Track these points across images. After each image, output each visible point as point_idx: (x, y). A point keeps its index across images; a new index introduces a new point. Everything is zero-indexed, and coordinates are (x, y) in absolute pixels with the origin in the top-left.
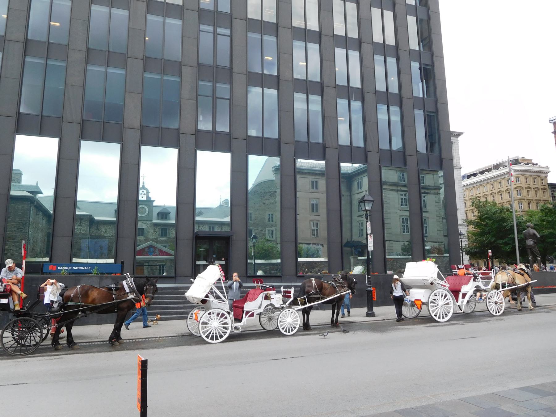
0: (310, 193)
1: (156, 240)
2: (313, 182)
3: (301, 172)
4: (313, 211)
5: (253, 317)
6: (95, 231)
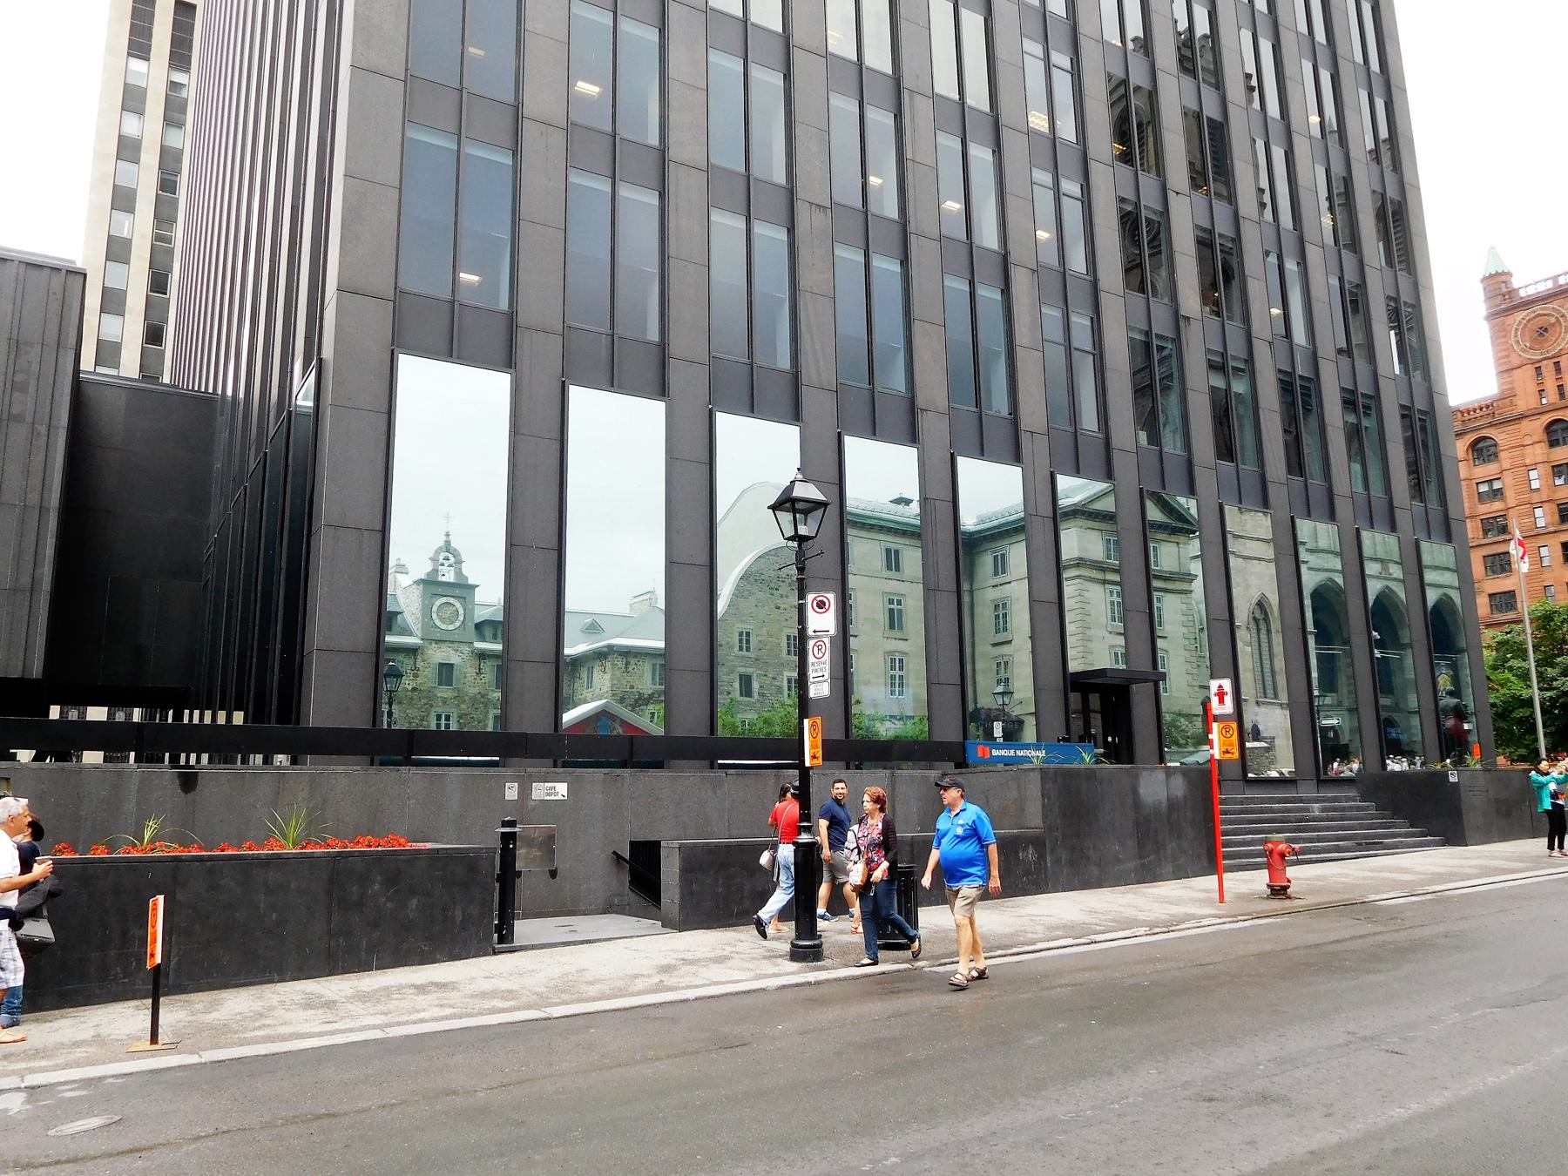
1: (482, 700)
2: (888, 551)
4: (892, 626)
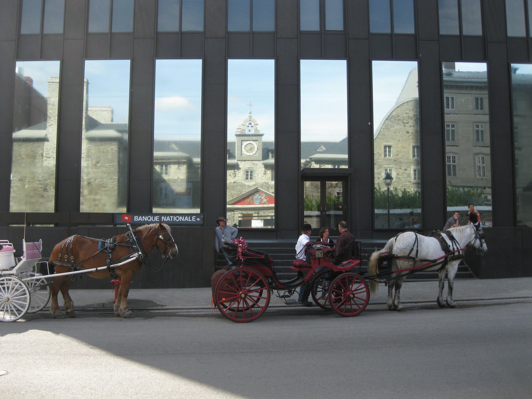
0: (473, 115)
1: (266, 185)
2: (477, 99)
3: (460, 86)
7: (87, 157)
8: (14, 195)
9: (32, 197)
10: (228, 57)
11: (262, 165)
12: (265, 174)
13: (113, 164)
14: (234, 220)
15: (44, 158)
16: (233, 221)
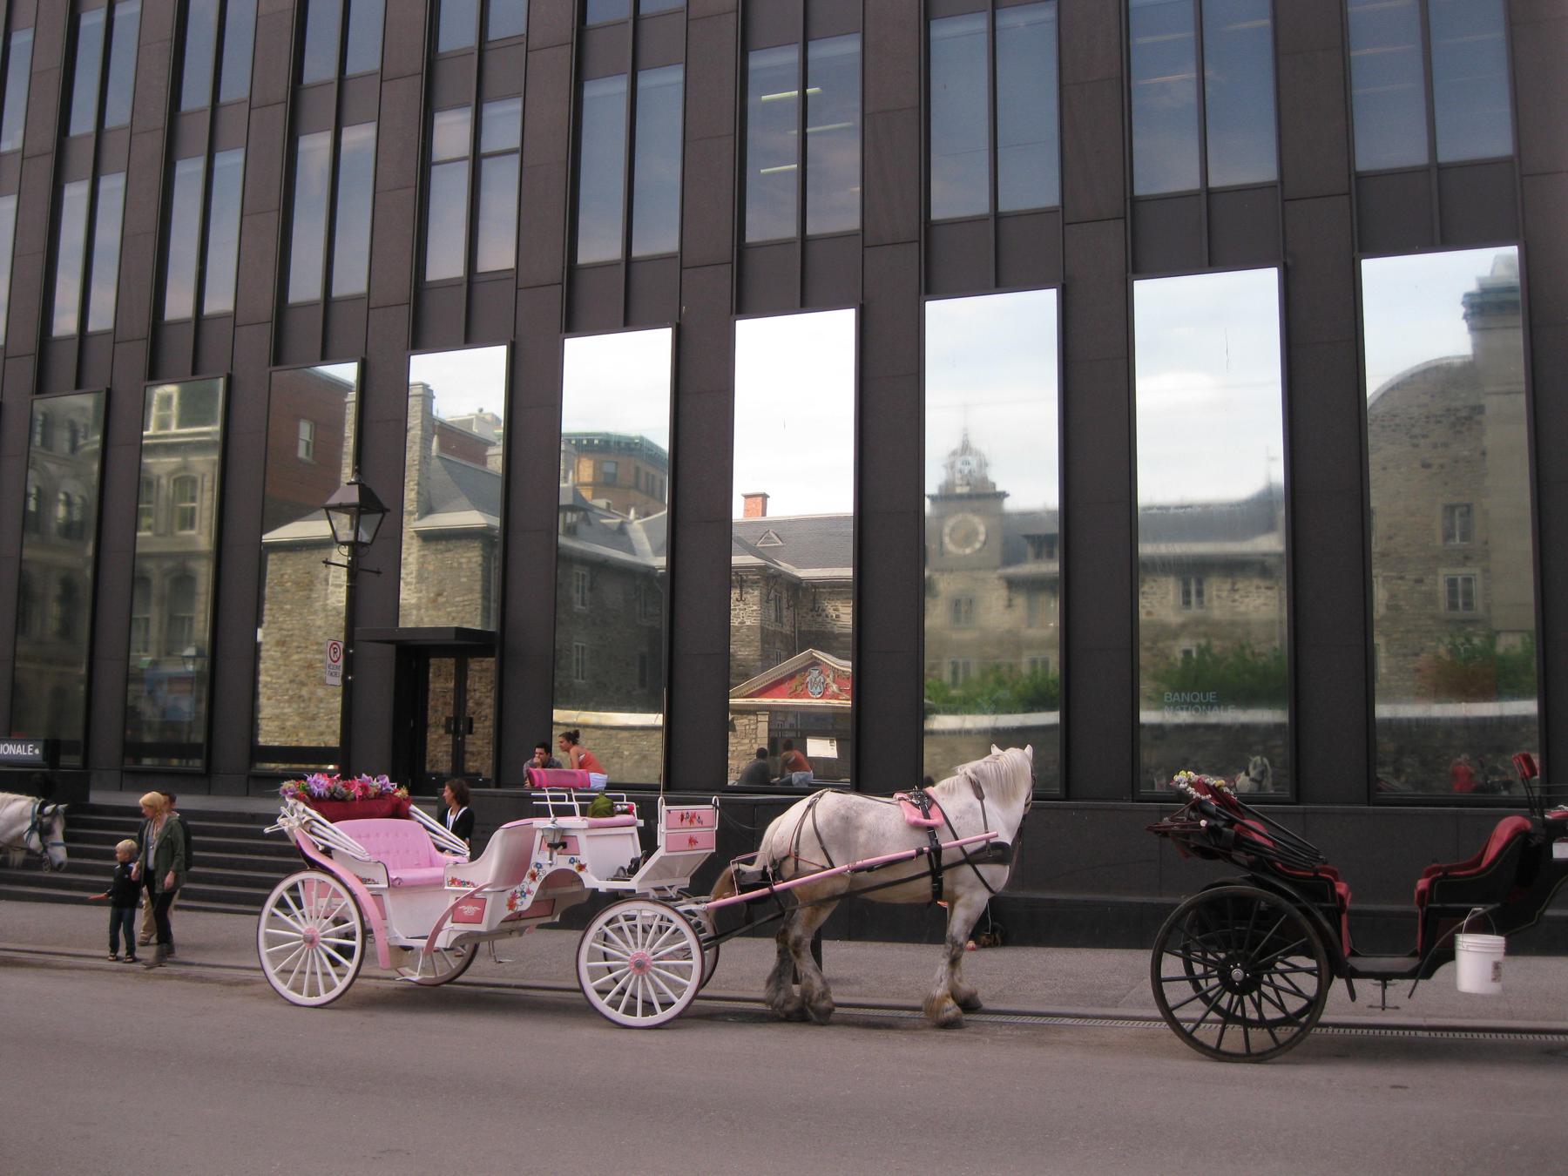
5: (480, 923)
6: (809, 617)
7: (418, 583)
8: (269, 679)
9: (303, 684)
10: (1361, 250)
11: (1001, 582)
12: (1010, 605)
13: (470, 597)
14: (755, 739)
15: (331, 588)
16: (753, 741)
